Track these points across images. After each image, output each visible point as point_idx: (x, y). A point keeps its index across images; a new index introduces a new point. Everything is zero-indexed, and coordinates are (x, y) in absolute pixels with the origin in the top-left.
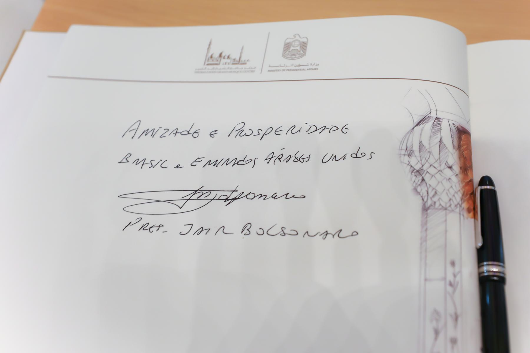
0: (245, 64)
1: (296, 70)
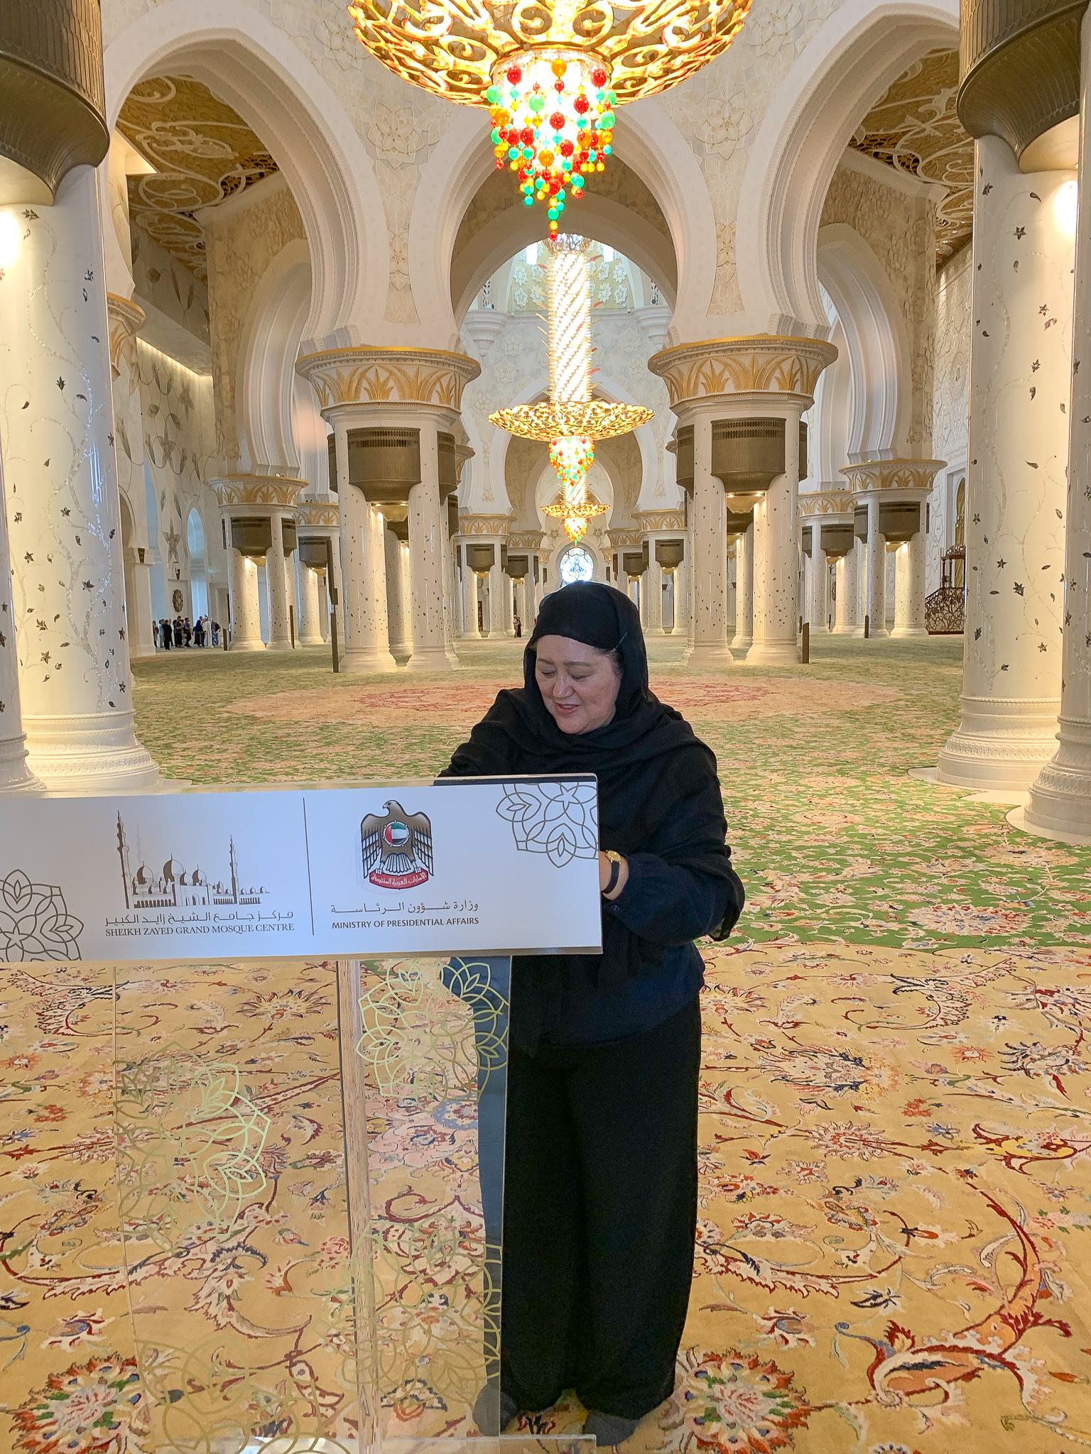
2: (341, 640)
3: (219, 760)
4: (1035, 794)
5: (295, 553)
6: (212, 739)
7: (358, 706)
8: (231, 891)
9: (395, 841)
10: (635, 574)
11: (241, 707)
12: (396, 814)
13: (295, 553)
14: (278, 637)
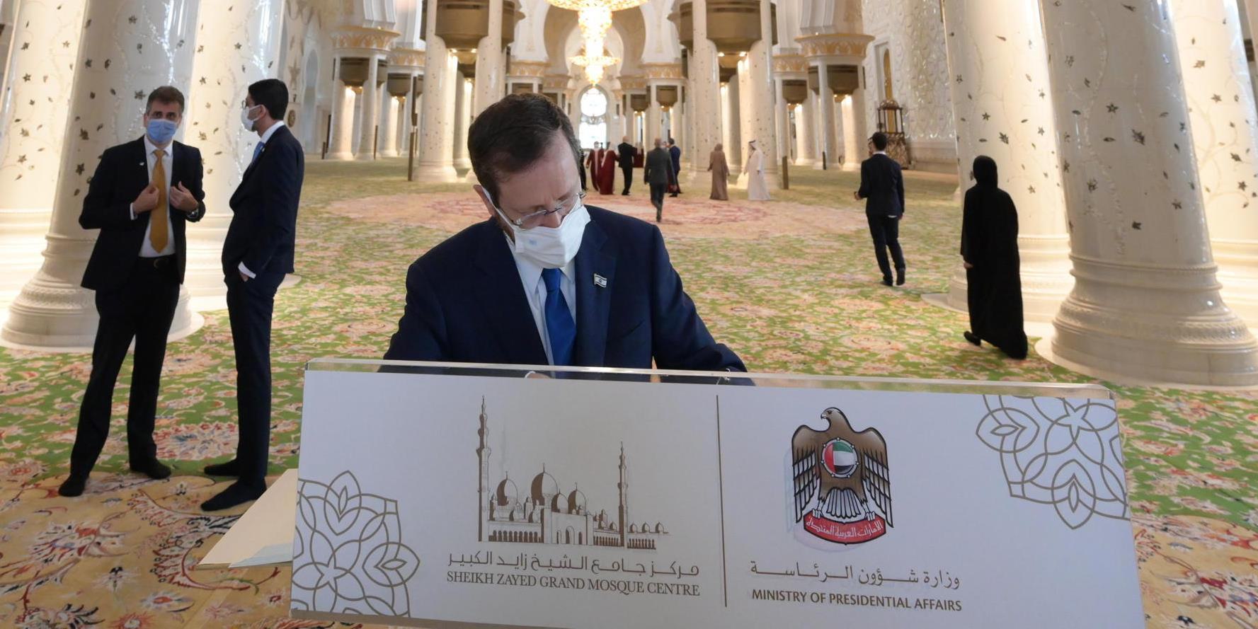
0: (650, 546)
1: (858, 601)
2: (417, 154)
3: (323, 258)
4: (1060, 327)
5: (383, 86)
6: (316, 237)
7: (431, 211)
8: (616, 526)
9: (839, 469)
10: (639, 111)
11: (338, 208)
12: (838, 428)
13: (383, 86)
14: (364, 149)
